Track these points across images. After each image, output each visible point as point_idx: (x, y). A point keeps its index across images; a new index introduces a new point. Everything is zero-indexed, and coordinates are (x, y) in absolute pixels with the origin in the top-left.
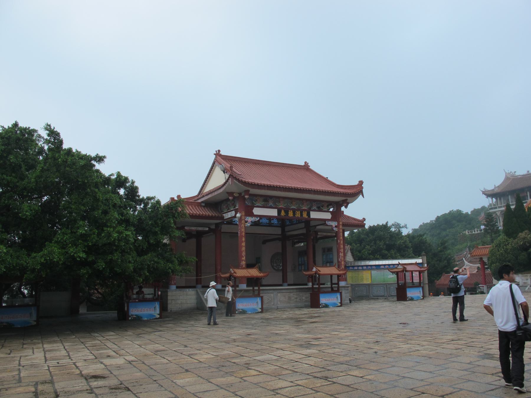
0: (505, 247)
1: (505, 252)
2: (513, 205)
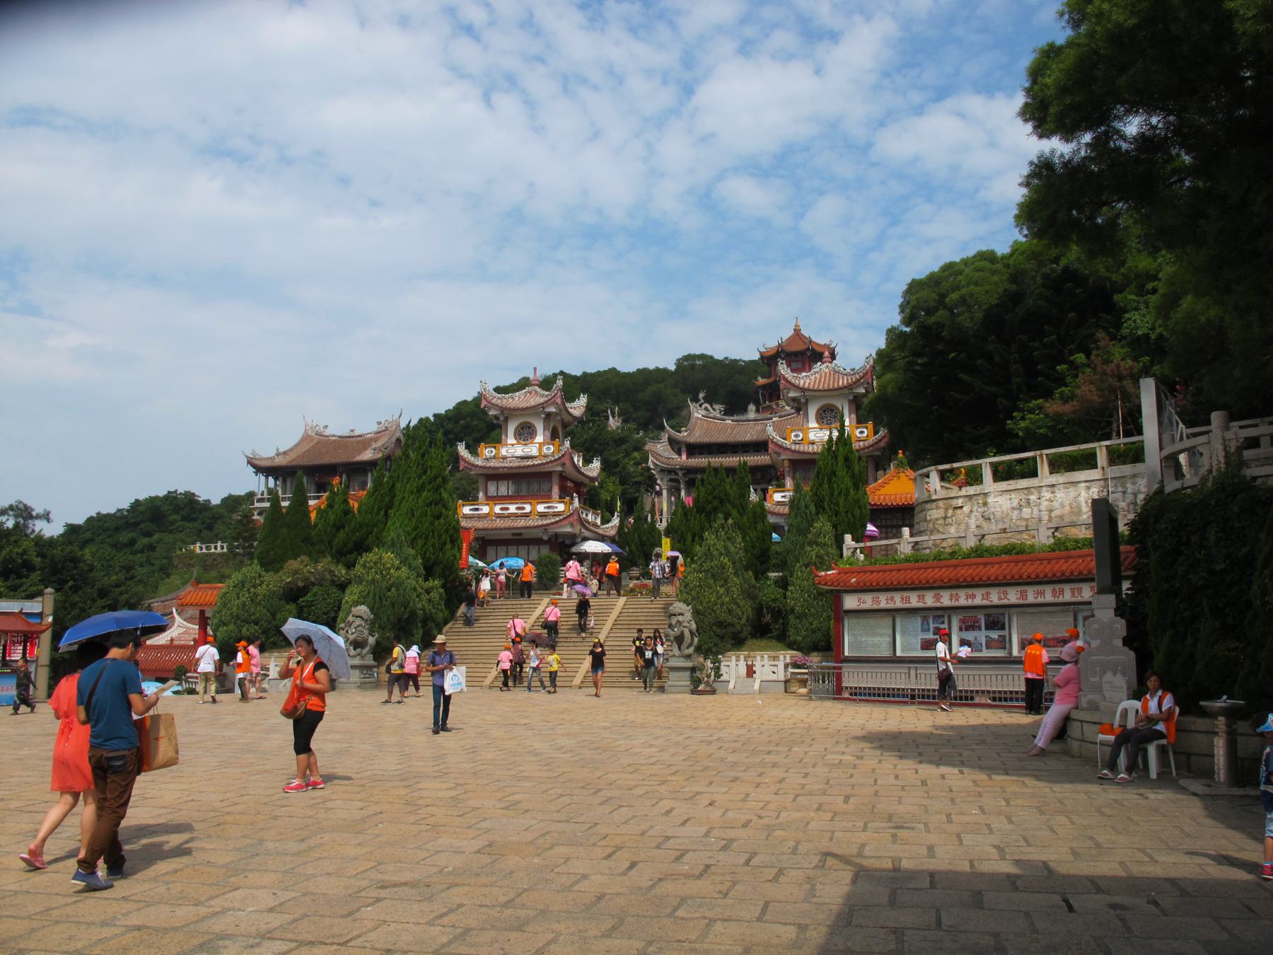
0: (252, 590)
1: (252, 600)
2: (284, 499)
